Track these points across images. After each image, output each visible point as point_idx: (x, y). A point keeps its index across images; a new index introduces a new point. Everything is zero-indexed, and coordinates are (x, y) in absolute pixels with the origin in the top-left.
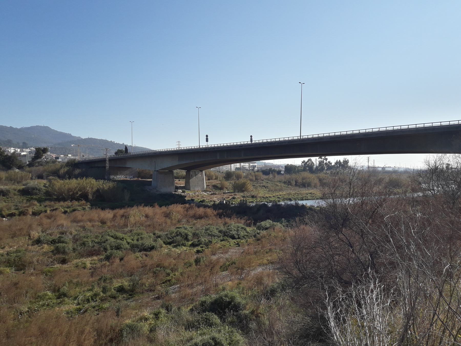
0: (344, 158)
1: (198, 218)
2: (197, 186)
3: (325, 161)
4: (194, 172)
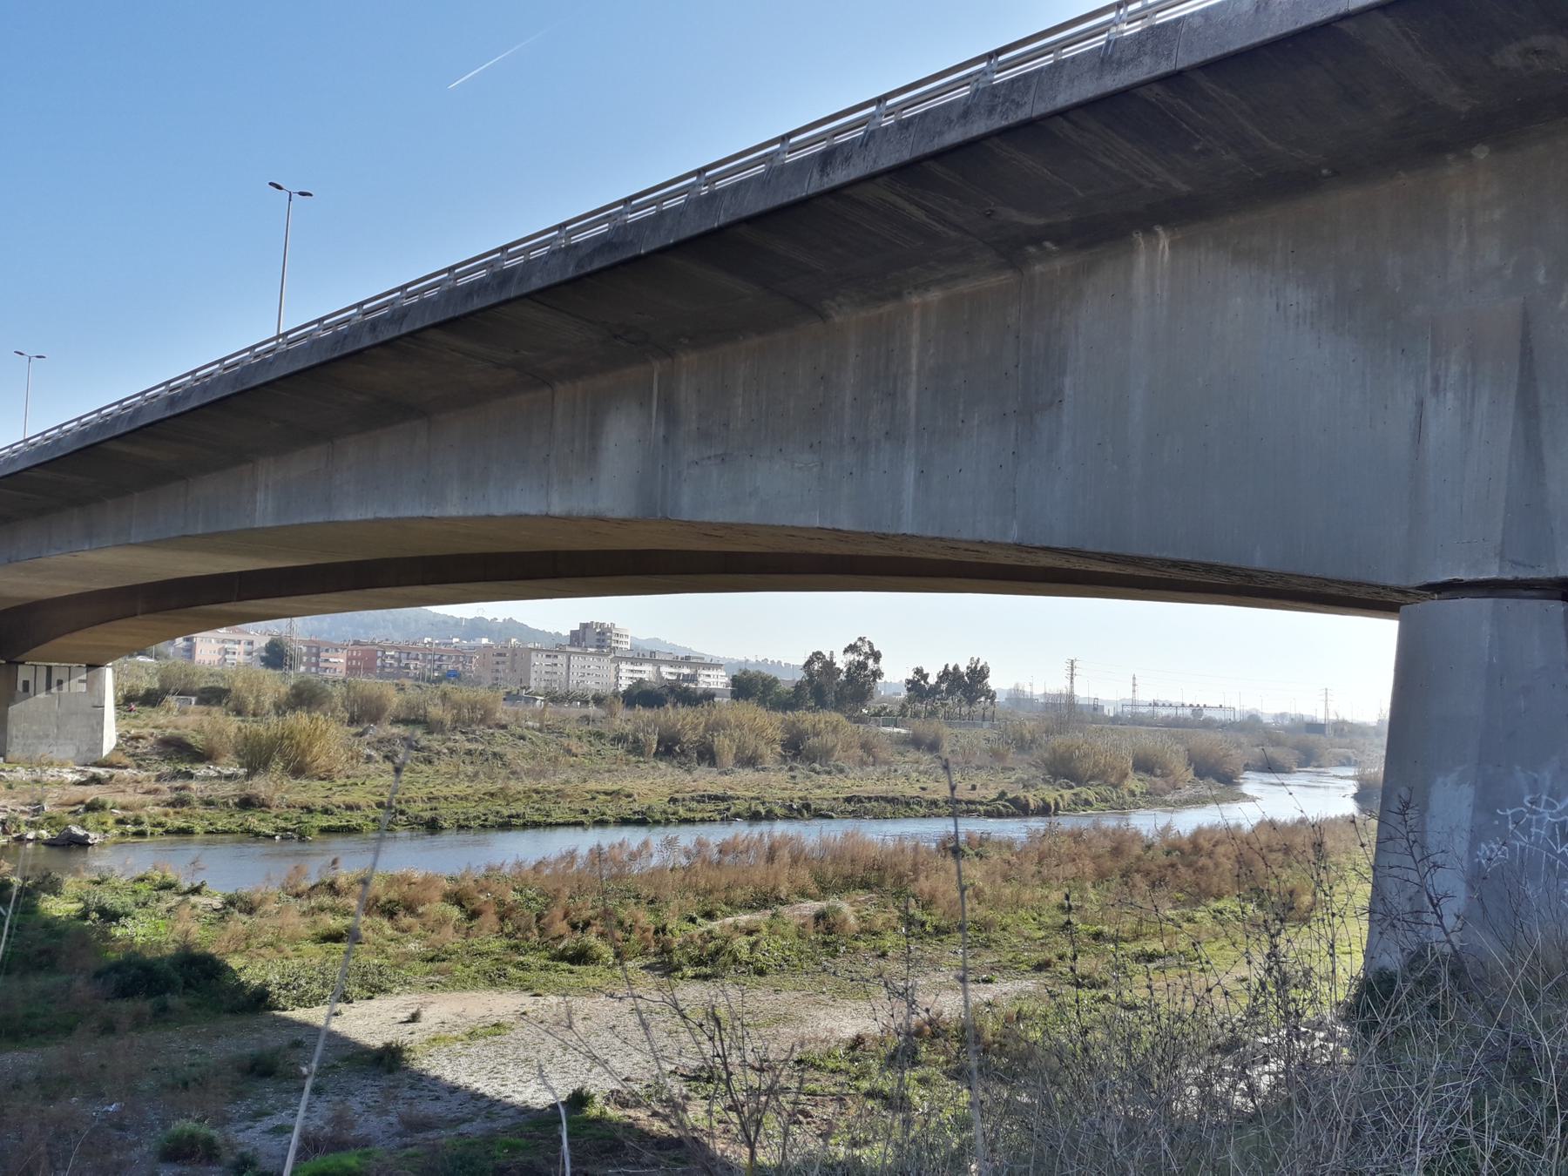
0: (972, 659)
1: (740, 908)
2: (57, 737)
3: (870, 662)
4: (42, 674)
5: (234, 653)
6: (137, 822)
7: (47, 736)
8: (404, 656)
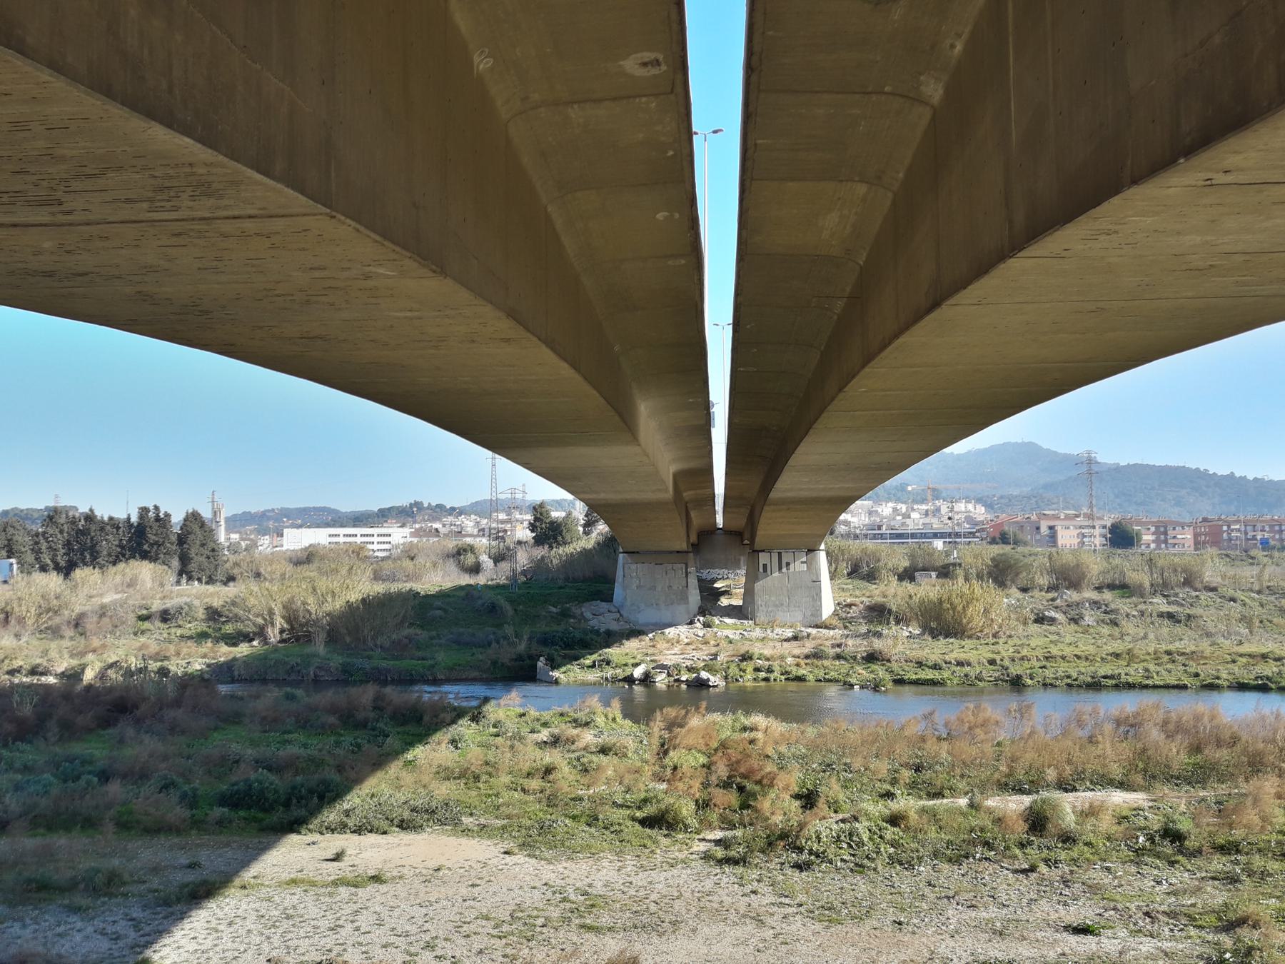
5: (1091, 536)
6: (770, 670)
7: (782, 605)
8: (1249, 528)
